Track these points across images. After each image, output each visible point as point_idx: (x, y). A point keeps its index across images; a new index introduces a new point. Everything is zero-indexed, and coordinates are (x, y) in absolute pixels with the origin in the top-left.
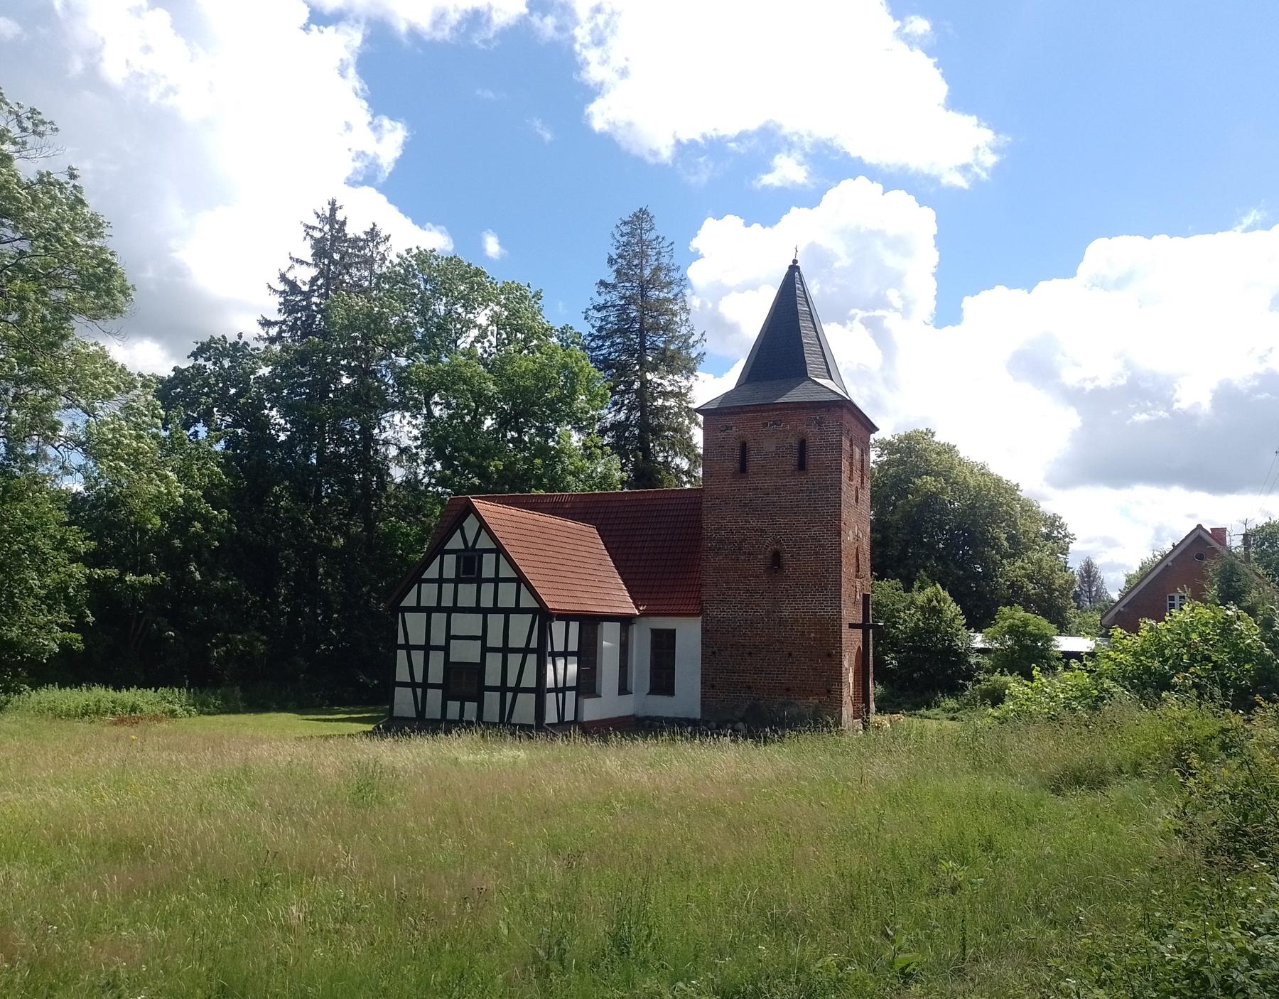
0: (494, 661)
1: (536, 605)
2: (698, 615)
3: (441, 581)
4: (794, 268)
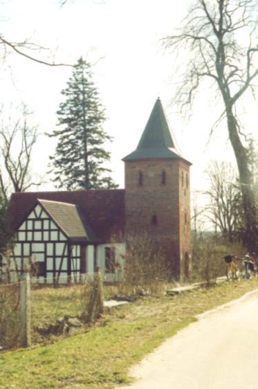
0: (50, 261)
3: (26, 231)
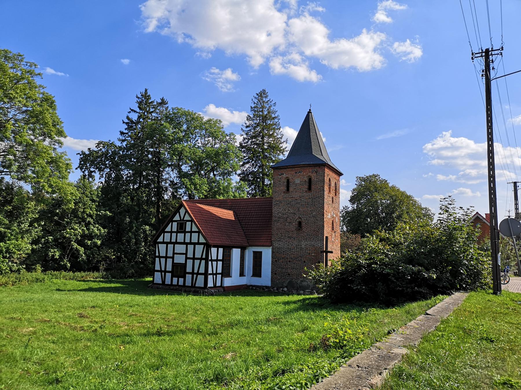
0: (190, 263)
1: (205, 242)
2: (270, 246)
3: (171, 232)
4: (309, 112)
